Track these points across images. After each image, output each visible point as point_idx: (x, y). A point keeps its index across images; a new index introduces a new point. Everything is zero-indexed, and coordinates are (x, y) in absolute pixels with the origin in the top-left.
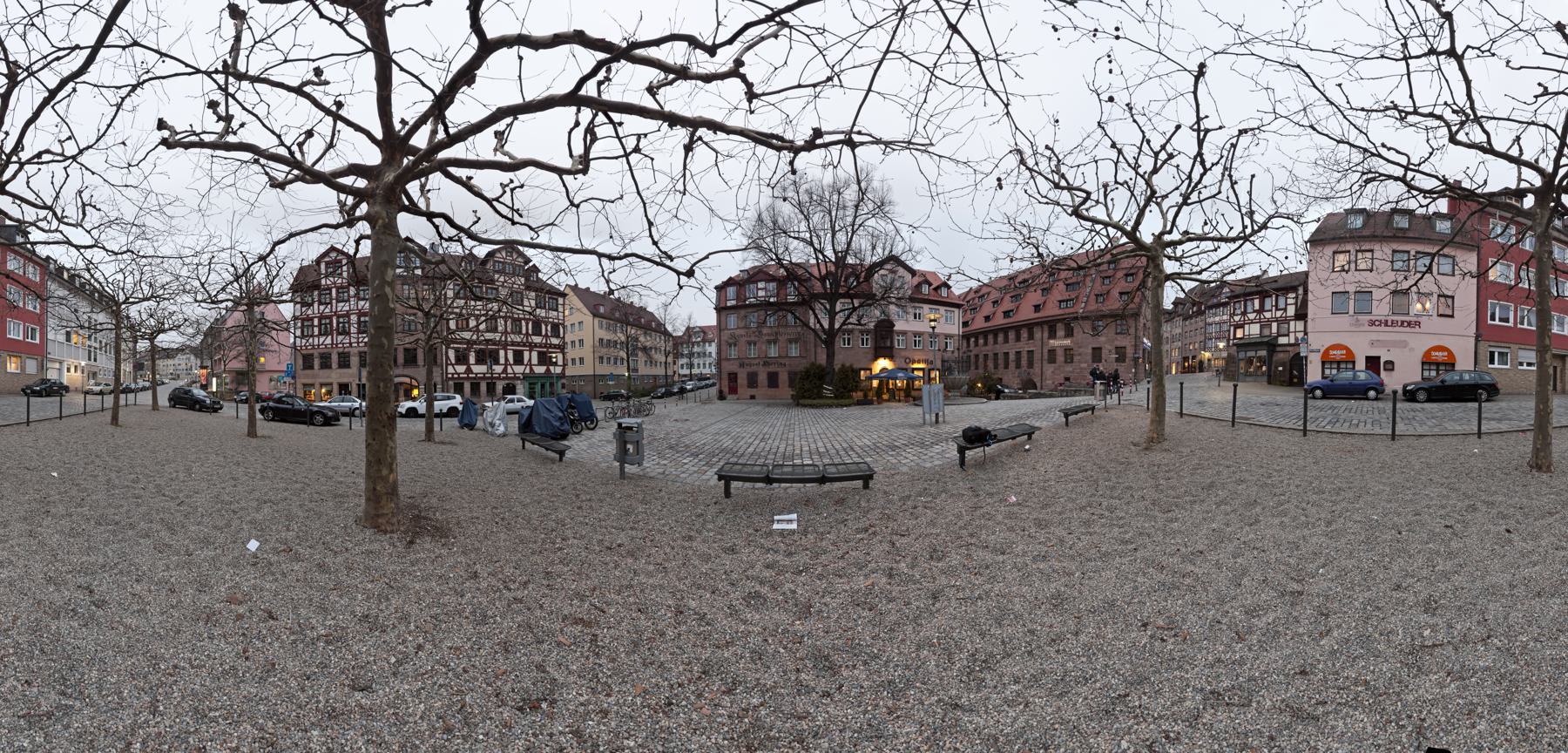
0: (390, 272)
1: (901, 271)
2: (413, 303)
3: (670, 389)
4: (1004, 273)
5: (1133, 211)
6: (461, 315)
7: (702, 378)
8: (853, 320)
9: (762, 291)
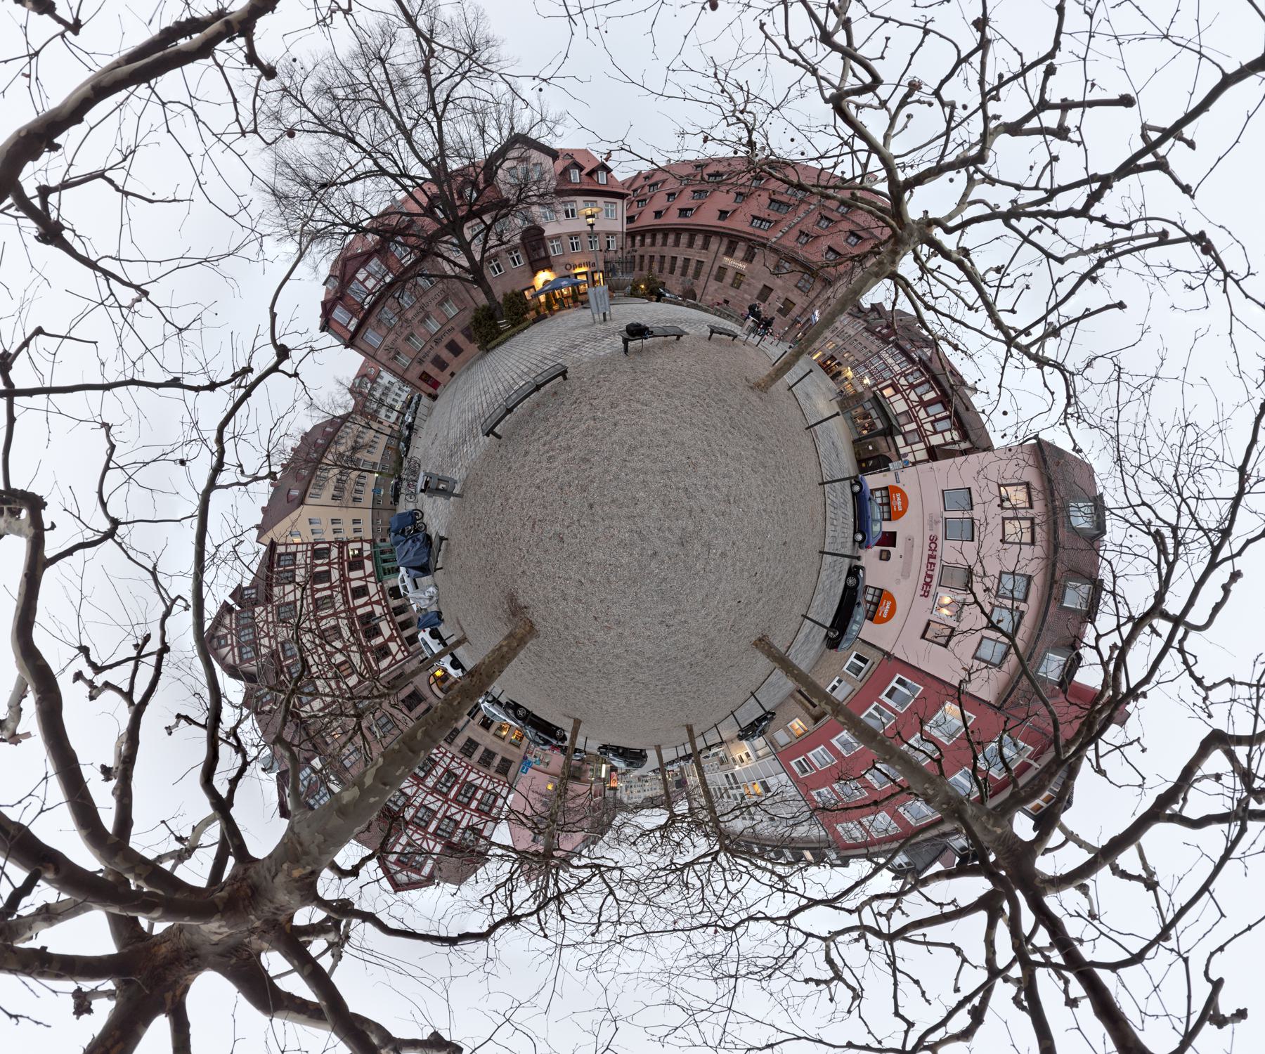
0: (347, 797)
1: (535, 155)
2: (358, 740)
3: (404, 437)
4: (691, 156)
5: (928, 158)
6: (336, 677)
7: (408, 404)
8: (493, 241)
9: (368, 280)
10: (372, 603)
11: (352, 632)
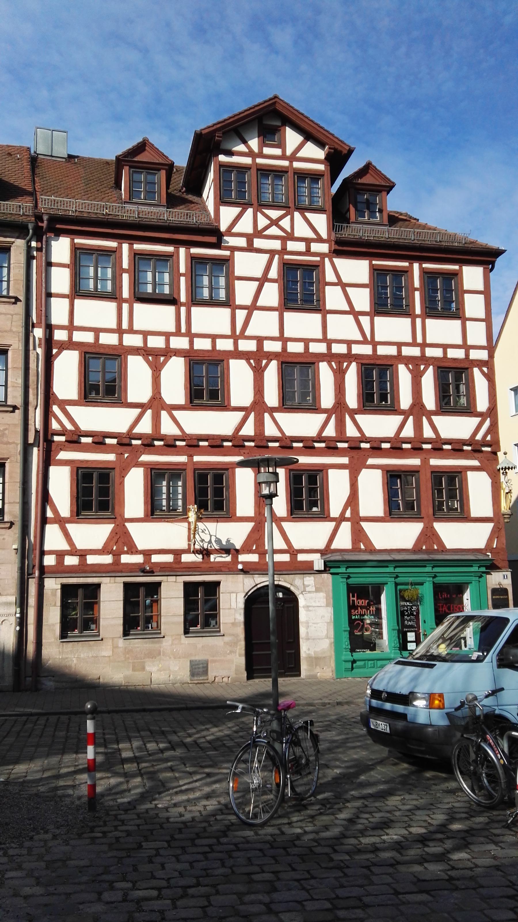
10: (258, 521)
11: (193, 443)
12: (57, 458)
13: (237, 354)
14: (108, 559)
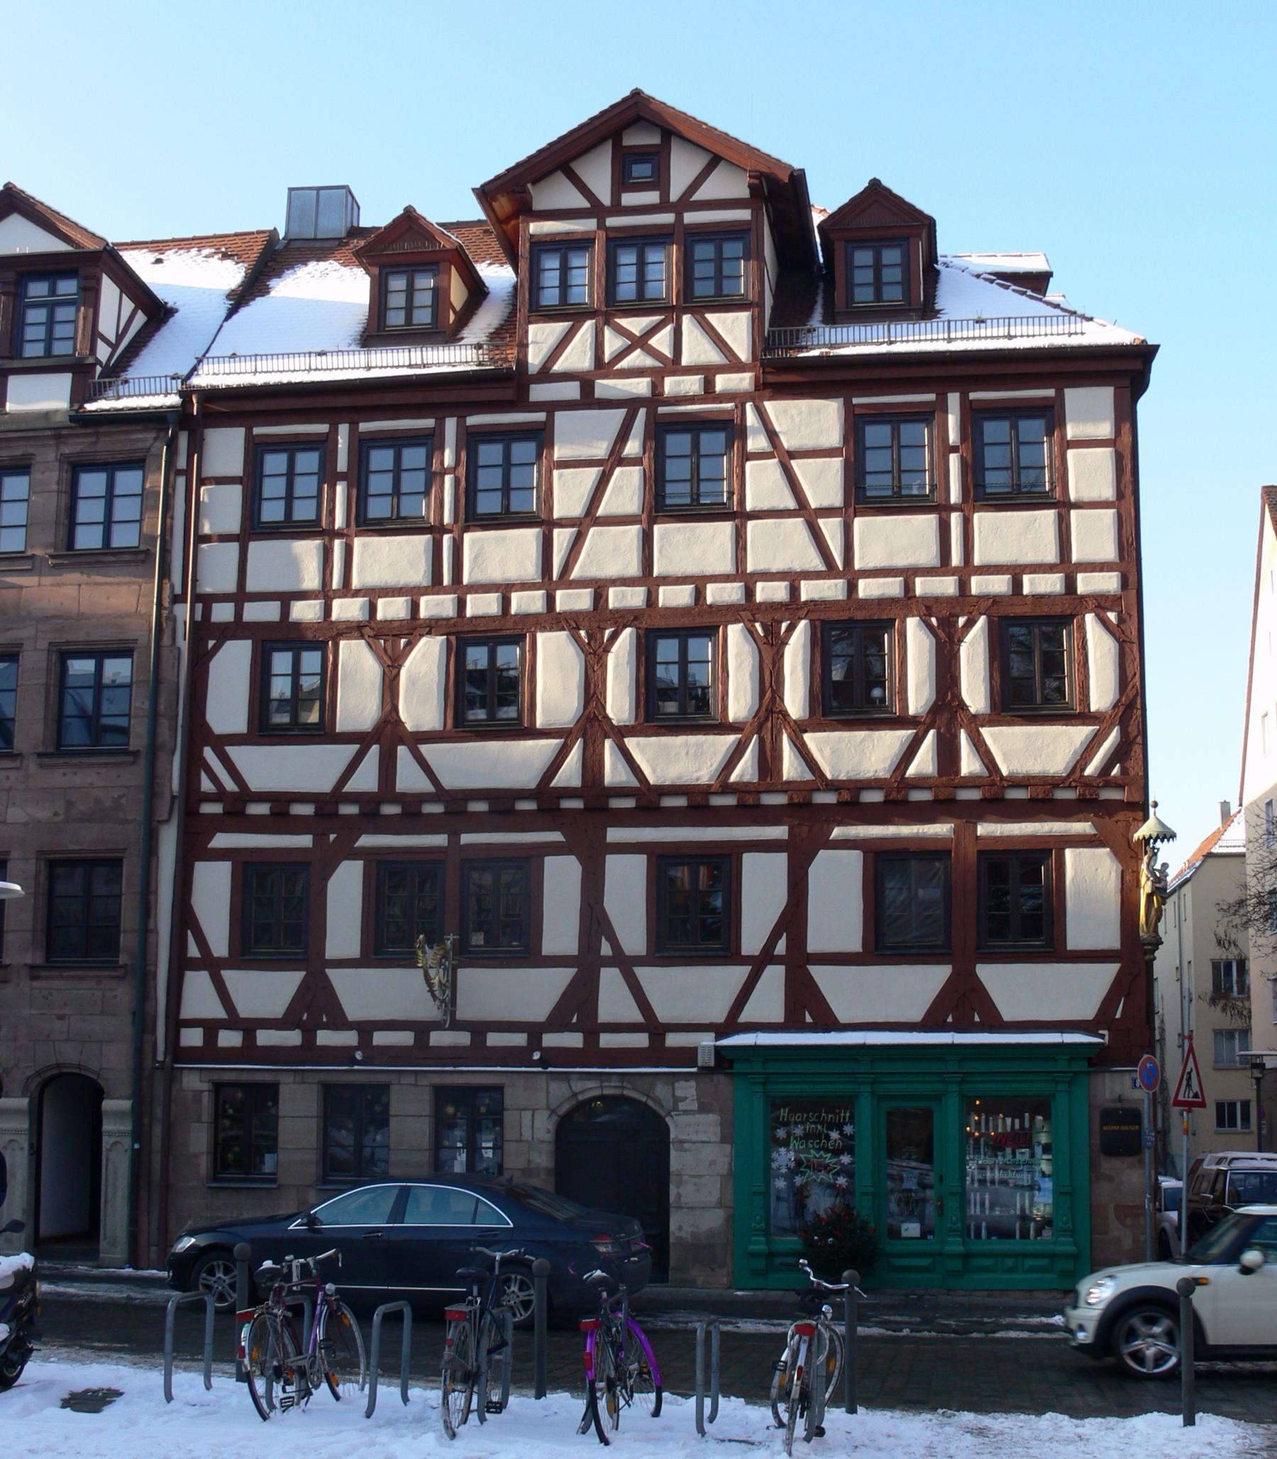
10: (586, 966)
11: (457, 806)
12: (211, 845)
13: (552, 619)
14: (292, 1038)
